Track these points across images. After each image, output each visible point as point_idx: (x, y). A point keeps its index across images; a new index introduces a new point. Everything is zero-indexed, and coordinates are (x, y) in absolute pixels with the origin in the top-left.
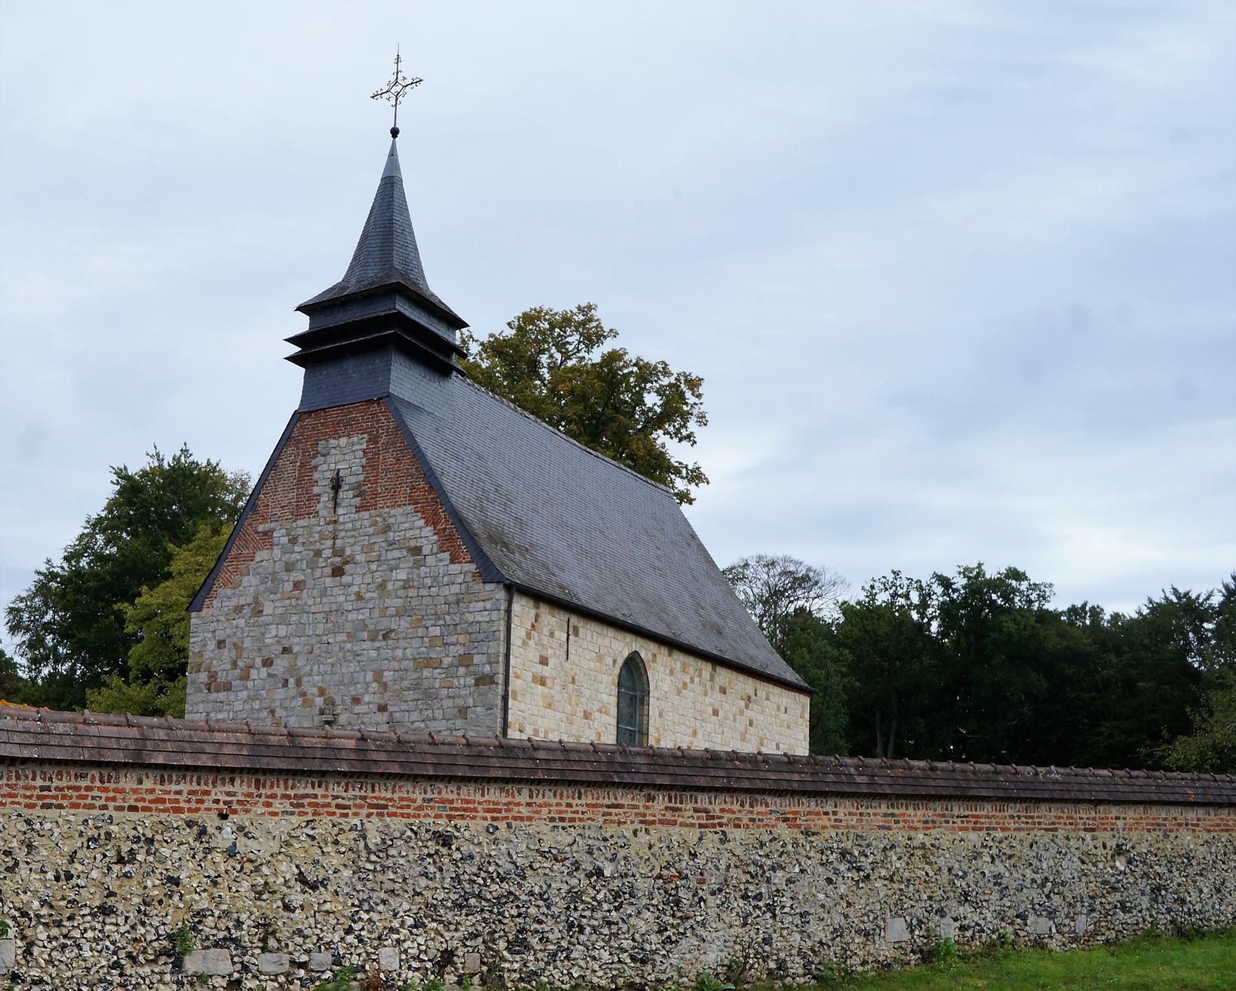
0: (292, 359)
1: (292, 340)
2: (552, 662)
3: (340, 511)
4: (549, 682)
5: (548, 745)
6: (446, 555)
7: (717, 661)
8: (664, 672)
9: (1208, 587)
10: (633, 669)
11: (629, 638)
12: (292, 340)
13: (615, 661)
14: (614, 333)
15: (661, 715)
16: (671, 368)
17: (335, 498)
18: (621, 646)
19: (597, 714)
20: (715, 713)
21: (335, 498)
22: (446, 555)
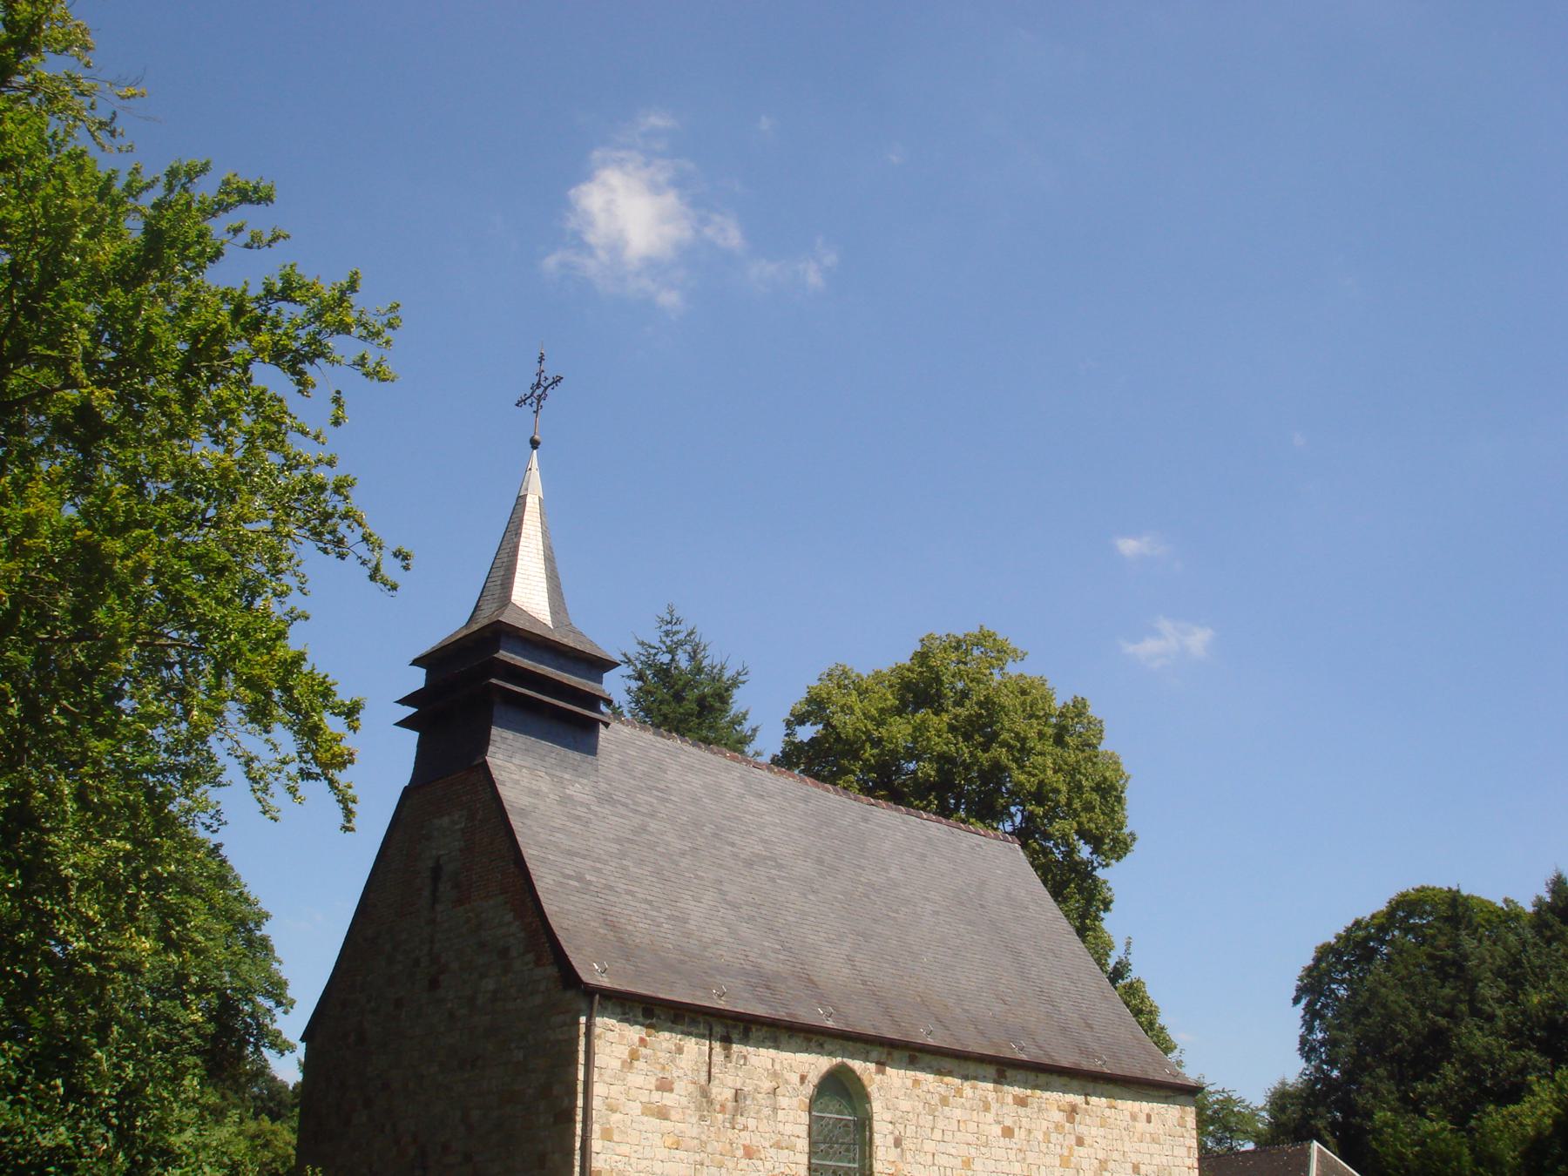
0: (405, 723)
1: (405, 701)
2: (679, 1086)
3: (439, 908)
4: (674, 1115)
5: (1110, 1087)
6: (530, 957)
7: (1003, 1069)
8: (892, 1091)
9: (1512, 879)
10: (840, 1089)
11: (820, 1049)
12: (405, 701)
13: (803, 1079)
14: (1019, 656)
15: (898, 1143)
16: (351, 492)
17: (435, 890)
18: (817, 1064)
19: (773, 1151)
20: (1008, 1132)
21: (435, 890)
22: (530, 957)
